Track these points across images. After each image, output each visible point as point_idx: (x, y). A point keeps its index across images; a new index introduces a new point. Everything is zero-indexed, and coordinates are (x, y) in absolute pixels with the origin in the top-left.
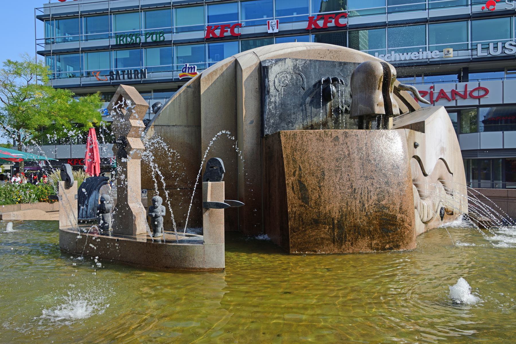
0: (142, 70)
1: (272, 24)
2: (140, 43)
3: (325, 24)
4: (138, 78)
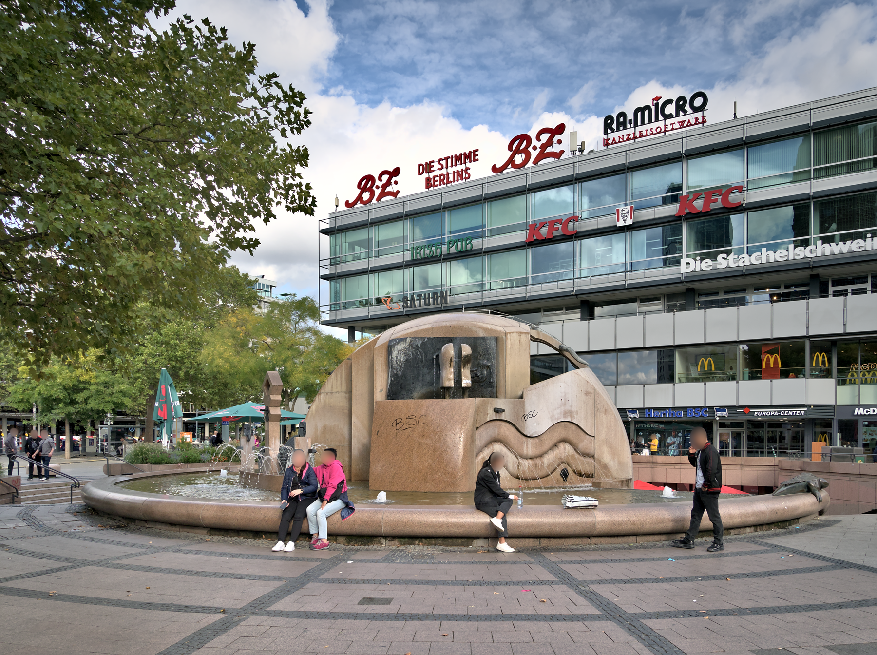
0: (442, 292)
1: (624, 212)
2: (441, 255)
3: (706, 204)
4: (438, 304)
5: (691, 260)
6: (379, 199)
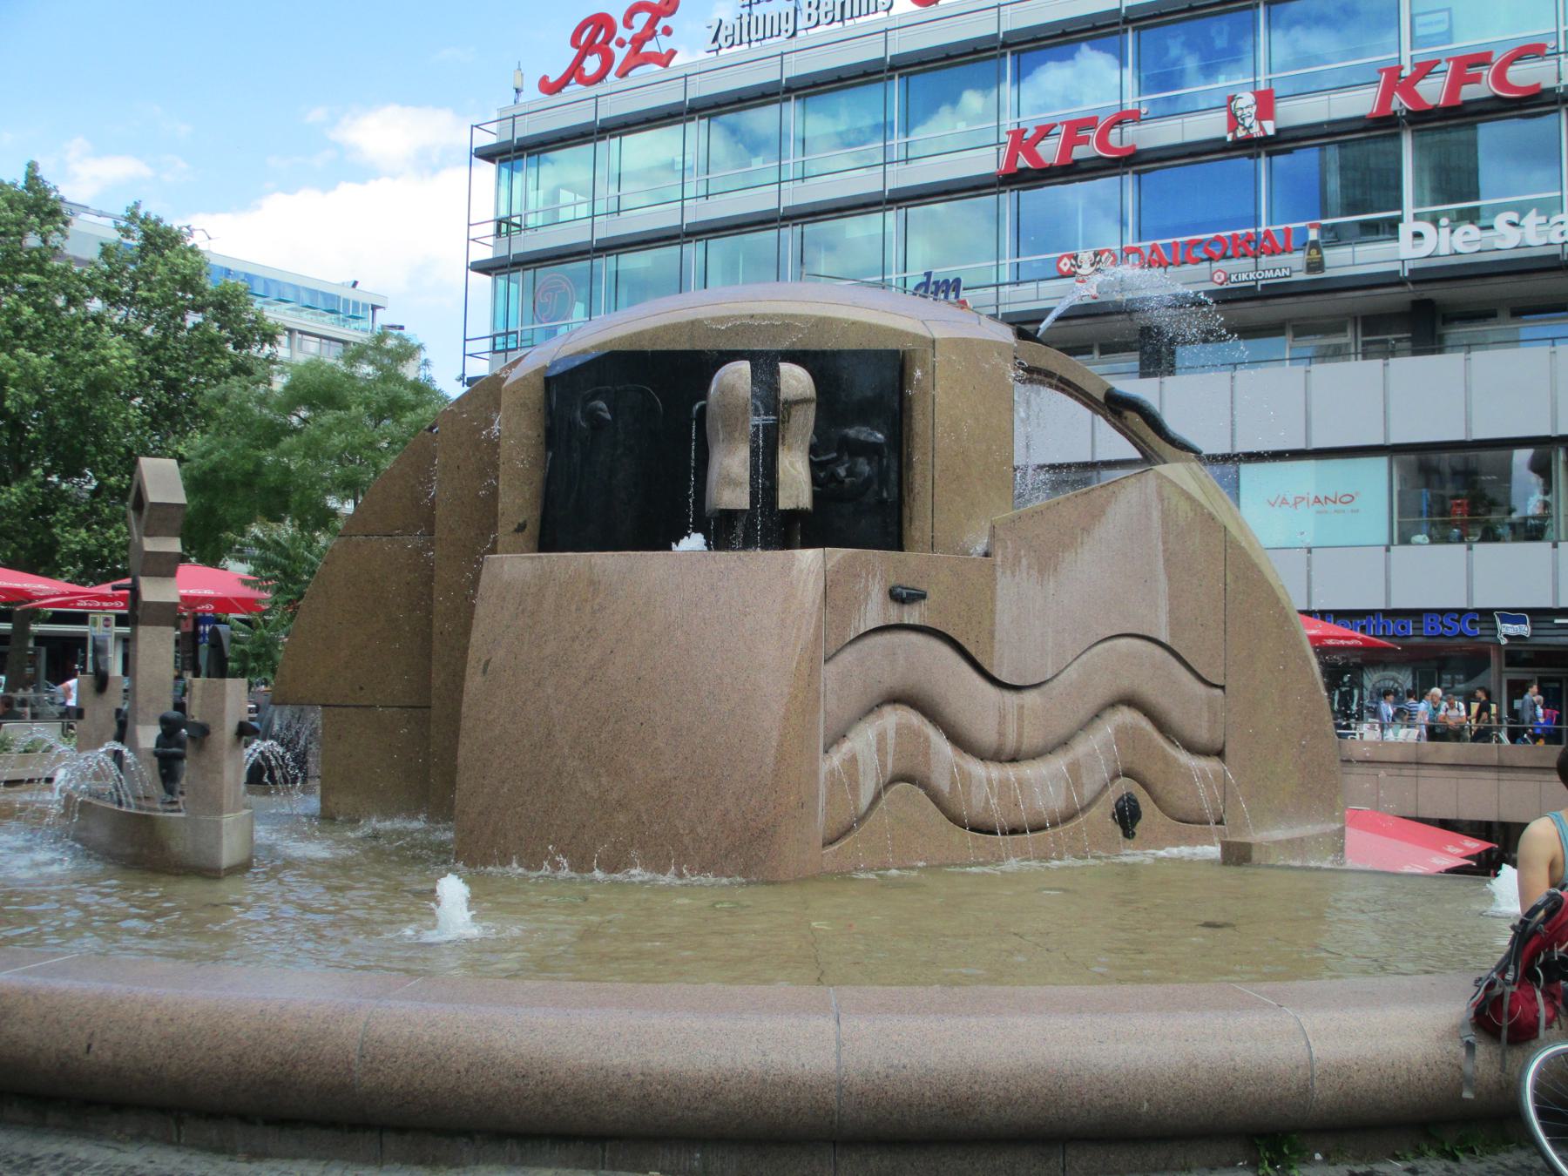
3: (1454, 87)
5: (1425, 227)
6: (623, 73)
